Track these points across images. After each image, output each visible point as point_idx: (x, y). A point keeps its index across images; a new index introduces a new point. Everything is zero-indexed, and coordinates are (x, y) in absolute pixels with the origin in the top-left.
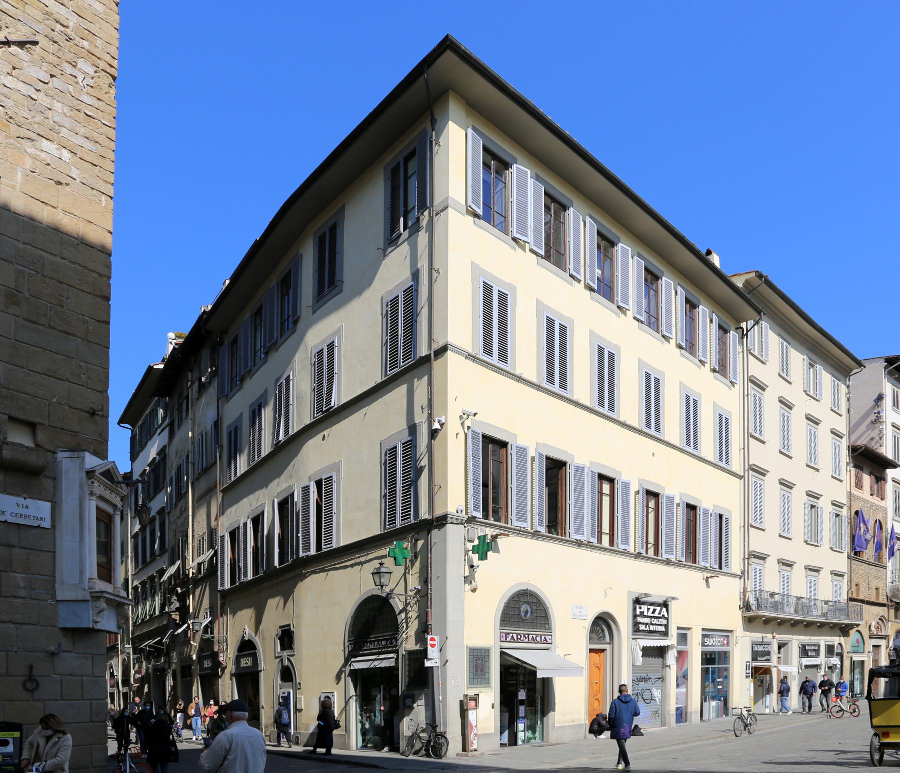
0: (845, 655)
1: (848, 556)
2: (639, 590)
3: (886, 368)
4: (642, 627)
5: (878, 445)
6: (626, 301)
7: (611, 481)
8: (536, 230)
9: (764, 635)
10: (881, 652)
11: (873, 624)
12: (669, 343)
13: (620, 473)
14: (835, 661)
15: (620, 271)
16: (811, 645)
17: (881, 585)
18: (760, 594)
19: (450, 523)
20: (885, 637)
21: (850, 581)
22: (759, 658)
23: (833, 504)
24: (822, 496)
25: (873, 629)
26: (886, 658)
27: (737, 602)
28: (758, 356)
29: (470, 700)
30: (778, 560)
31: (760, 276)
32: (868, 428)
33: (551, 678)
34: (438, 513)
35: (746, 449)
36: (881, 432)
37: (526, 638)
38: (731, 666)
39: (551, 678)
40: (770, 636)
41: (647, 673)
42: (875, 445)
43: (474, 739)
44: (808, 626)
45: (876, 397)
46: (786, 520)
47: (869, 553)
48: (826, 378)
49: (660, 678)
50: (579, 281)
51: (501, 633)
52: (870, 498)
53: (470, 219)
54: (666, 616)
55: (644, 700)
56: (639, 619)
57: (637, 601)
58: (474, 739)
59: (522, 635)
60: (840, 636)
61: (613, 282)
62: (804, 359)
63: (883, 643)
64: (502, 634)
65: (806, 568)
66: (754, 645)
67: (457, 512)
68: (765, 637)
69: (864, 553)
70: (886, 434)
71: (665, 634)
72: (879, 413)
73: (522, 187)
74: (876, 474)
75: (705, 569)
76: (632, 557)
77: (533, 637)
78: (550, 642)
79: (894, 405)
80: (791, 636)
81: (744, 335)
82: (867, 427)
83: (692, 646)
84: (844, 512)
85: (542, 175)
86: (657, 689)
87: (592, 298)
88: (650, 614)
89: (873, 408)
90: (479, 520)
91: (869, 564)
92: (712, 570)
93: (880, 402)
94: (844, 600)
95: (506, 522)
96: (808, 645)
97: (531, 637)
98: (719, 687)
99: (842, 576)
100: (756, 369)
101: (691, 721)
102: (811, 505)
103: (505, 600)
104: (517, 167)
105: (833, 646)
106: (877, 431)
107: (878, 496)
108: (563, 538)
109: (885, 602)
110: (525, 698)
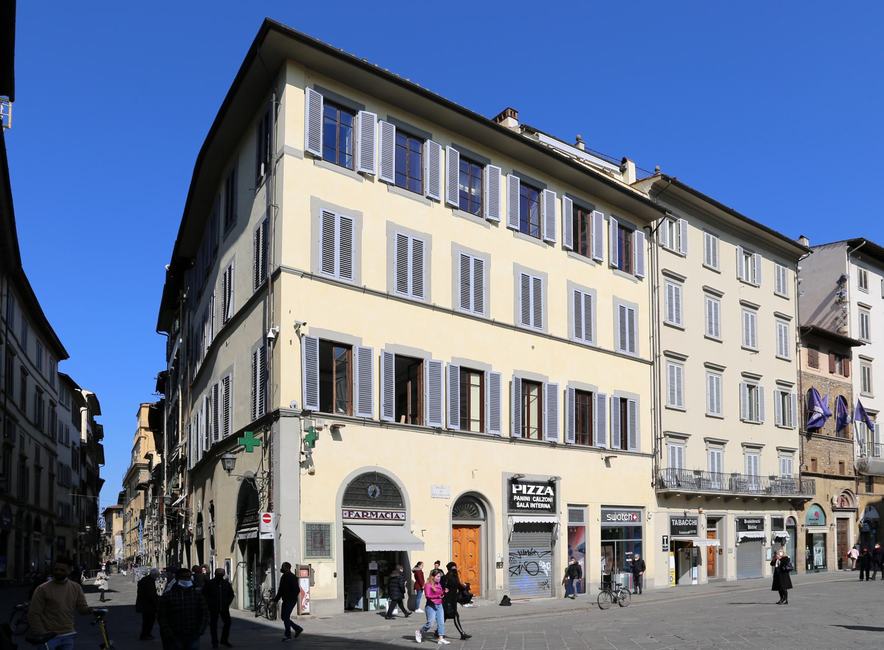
0: (799, 528)
1: (800, 432)
2: (515, 470)
3: (848, 251)
4: (519, 505)
5: (842, 324)
6: (496, 214)
7: (539, 384)
8: (385, 163)
9: (687, 510)
10: (849, 524)
11: (835, 497)
12: (642, 281)
13: (597, 387)
14: (783, 534)
15: (594, 232)
16: (752, 519)
17: (846, 459)
18: (680, 473)
19: (282, 416)
20: (855, 510)
21: (802, 457)
22: (680, 532)
23: (778, 383)
24: (762, 376)
25: (835, 502)
26: (855, 530)
27: (650, 480)
28: (752, 283)
29: (301, 569)
30: (742, 444)
31: (666, 178)
32: (832, 308)
33: (406, 552)
34: (273, 409)
35: (655, 337)
36: (844, 311)
37: (373, 515)
38: (643, 540)
39: (406, 552)
40: (697, 511)
41: (532, 547)
42: (839, 325)
43: (306, 604)
44: (747, 502)
45: (838, 278)
46: (715, 401)
47: (830, 427)
48: (767, 266)
49: (550, 552)
50: (438, 202)
51: (343, 510)
52: (830, 376)
53: (311, 161)
54: (552, 494)
55: (528, 572)
56: (515, 497)
57: (514, 481)
58: (306, 604)
59: (369, 513)
60: (791, 510)
61: (482, 199)
62: (737, 249)
63: (851, 516)
64: (345, 512)
65: (706, 440)
66: (673, 521)
67: (291, 407)
68: (687, 512)
69: (823, 430)
70: (850, 313)
71: (553, 510)
72: (841, 294)
73: (368, 130)
74: (836, 352)
75: (603, 450)
76: (506, 441)
77: (382, 514)
78: (403, 518)
79: (861, 285)
80: (725, 511)
81: (650, 233)
82: (831, 307)
83: (589, 522)
84: (794, 391)
85: (569, 192)
86: (546, 562)
87: (454, 215)
88: (530, 492)
89: (837, 289)
90: (457, 431)
91: (830, 439)
92: (612, 451)
93: (843, 284)
94: (795, 474)
95: (351, 415)
96: (747, 519)
97: (379, 514)
98: (627, 560)
99: (792, 451)
100: (667, 261)
101: (589, 593)
102: (782, 393)
103: (349, 481)
104: (362, 113)
105: (782, 520)
106: (841, 311)
107: (841, 374)
108: (422, 426)
109: (853, 475)
110: (377, 569)
